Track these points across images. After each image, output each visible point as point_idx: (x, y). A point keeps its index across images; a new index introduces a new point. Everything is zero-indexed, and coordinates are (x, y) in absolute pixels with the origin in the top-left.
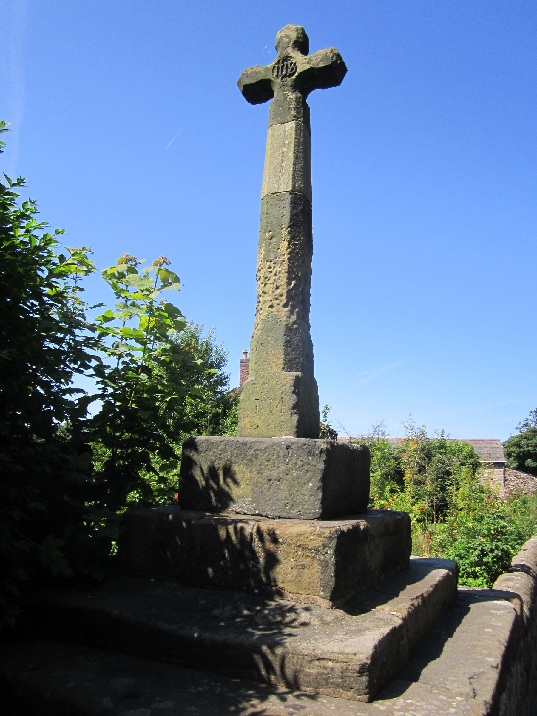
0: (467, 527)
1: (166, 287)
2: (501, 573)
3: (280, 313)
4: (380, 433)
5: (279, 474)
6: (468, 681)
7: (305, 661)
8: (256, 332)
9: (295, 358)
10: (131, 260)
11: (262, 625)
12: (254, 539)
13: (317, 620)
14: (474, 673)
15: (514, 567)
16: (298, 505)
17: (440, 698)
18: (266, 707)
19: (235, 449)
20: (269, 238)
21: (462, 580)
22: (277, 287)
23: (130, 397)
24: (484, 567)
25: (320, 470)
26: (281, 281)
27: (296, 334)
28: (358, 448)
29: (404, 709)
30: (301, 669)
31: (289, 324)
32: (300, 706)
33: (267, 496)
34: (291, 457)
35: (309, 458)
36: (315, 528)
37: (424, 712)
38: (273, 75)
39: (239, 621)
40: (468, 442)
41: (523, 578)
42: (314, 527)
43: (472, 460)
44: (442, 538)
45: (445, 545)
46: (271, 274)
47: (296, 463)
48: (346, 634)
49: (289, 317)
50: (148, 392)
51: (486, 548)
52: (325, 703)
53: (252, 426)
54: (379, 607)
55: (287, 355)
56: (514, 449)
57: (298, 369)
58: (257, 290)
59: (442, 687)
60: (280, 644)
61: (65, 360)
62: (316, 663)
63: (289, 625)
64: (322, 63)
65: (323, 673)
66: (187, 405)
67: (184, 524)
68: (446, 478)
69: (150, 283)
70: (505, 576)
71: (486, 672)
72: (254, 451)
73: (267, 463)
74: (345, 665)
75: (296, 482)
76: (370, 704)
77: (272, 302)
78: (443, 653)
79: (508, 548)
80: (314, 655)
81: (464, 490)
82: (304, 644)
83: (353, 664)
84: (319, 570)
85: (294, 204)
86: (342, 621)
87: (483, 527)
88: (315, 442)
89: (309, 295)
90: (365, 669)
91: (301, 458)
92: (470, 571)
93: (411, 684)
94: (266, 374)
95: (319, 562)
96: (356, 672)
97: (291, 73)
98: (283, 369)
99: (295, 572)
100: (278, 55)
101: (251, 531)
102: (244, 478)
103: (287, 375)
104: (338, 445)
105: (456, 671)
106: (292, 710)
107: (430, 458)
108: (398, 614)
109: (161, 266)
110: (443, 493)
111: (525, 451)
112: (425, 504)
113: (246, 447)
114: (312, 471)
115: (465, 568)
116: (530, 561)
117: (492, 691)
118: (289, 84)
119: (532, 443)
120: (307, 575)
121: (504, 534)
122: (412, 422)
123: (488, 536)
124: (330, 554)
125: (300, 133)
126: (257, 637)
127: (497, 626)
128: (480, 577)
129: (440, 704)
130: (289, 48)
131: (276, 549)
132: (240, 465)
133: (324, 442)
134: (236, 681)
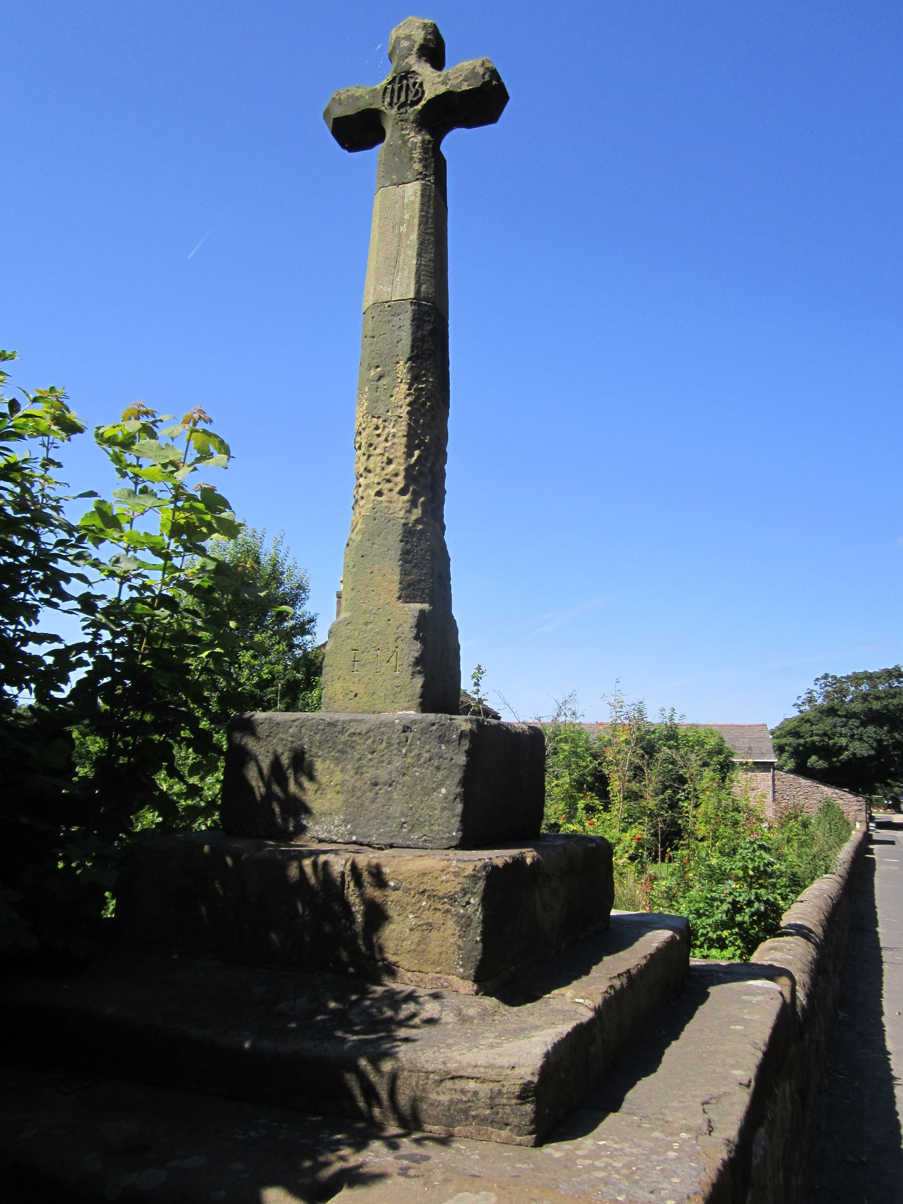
0: (709, 866)
1: (205, 460)
2: (764, 939)
3: (395, 505)
4: (569, 713)
5: (390, 773)
6: (701, 1109)
7: (430, 1082)
8: (353, 536)
9: (420, 581)
10: (146, 413)
11: (359, 1025)
12: (347, 883)
13: (452, 1015)
14: (710, 1095)
15: (785, 928)
16: (421, 825)
17: (653, 1135)
18: (364, 1160)
19: (316, 733)
20: (376, 378)
21: (701, 952)
22: (390, 461)
23: (139, 648)
24: (737, 930)
25: (460, 766)
26: (396, 451)
27: (419, 540)
28: (524, 731)
29: (595, 1154)
30: (423, 1095)
31: (408, 523)
32: (421, 1156)
33: (371, 812)
34: (411, 745)
35: (440, 747)
36: (450, 862)
37: (627, 1159)
38: (383, 102)
39: (321, 1021)
40: (714, 728)
41: (799, 945)
42: (449, 860)
43: (721, 758)
44: (668, 885)
45: (674, 896)
46: (380, 439)
47: (419, 755)
48: (500, 1036)
49: (409, 511)
50: (172, 640)
51: (740, 899)
52: (462, 1149)
53: (347, 694)
54: (556, 992)
55: (405, 574)
56: (790, 740)
57: (424, 598)
58: (356, 466)
59: (658, 1119)
60: (389, 1054)
61: (26, 586)
62: (449, 1084)
63: (406, 1023)
64: (466, 84)
65: (460, 1101)
66: (243, 667)
67: (229, 860)
68: (679, 788)
69: (176, 455)
70: (769, 942)
71: (729, 1094)
72: (349, 735)
73: (370, 756)
74: (496, 1087)
75: (419, 788)
76: (538, 1148)
77: (380, 487)
78: (661, 1066)
79: (776, 899)
80: (445, 1072)
81: (708, 805)
82: (429, 1054)
83: (509, 1083)
84: (456, 932)
85: (418, 320)
86: (493, 1014)
87: (735, 865)
88: (451, 719)
89: (443, 475)
90: (530, 1091)
91: (427, 747)
92: (715, 936)
93: (607, 1115)
94: (371, 608)
95: (455, 918)
96: (514, 1098)
97: (415, 99)
98: (399, 598)
99: (416, 936)
100: (392, 69)
101: (342, 869)
102: (331, 781)
103: (406, 609)
104: (491, 725)
105: (681, 1092)
106: (407, 1162)
107: (651, 756)
108: (587, 1002)
109: (195, 424)
110: (673, 812)
111: (806, 742)
112: (644, 831)
113: (335, 730)
114: (445, 768)
115: (705, 932)
116: (811, 919)
117: (739, 1123)
118: (412, 118)
119: (819, 730)
120: (435, 941)
121: (771, 876)
122: (620, 695)
123: (744, 878)
124: (474, 905)
125: (429, 201)
126: (349, 1044)
127: (751, 1020)
128: (730, 946)
129: (652, 1145)
130: (412, 57)
131: (384, 898)
132: (324, 760)
133: (466, 720)
134: (315, 1119)
